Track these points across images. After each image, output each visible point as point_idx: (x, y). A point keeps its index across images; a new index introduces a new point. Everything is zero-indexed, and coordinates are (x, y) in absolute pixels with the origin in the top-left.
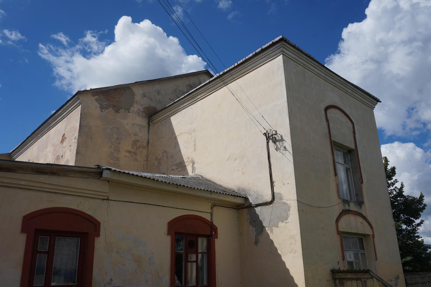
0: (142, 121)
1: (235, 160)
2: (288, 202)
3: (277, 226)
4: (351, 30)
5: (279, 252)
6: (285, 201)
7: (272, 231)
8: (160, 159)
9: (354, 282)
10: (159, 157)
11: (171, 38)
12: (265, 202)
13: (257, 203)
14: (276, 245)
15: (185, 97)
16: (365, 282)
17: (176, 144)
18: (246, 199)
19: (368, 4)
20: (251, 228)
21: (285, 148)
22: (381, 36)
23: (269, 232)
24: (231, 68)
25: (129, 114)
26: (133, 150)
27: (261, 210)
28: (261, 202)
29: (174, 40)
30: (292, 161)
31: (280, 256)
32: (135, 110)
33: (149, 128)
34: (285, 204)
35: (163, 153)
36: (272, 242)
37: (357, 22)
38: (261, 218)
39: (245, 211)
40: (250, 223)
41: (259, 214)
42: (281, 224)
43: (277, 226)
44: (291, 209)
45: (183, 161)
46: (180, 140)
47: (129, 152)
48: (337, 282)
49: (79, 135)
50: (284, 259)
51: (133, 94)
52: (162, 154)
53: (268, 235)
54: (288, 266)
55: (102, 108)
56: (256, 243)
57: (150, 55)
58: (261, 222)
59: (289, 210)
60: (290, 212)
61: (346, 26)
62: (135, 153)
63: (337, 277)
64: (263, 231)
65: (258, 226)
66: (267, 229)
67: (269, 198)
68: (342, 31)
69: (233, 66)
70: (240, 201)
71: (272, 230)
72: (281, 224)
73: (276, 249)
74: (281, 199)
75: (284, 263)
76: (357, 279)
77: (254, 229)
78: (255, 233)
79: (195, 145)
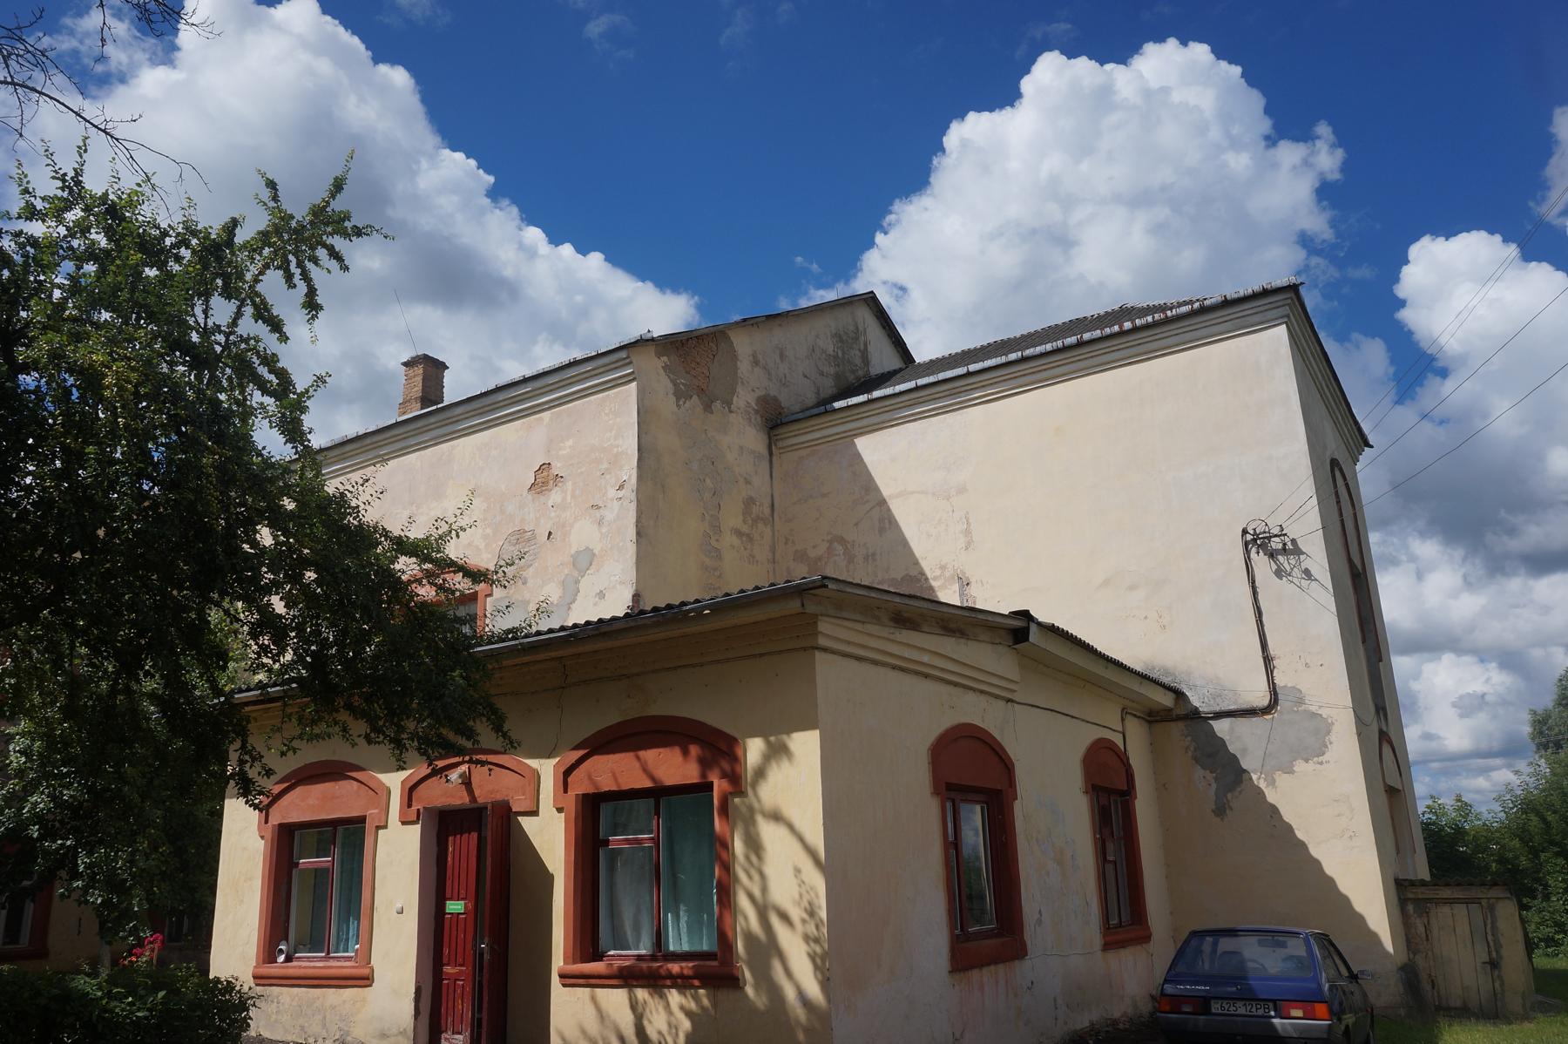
0: (753, 438)
1: (1132, 588)
2: (1324, 712)
3: (1290, 771)
4: (970, 132)
5: (1300, 835)
6: (1313, 709)
7: (1272, 783)
8: (820, 559)
9: (1461, 910)
10: (812, 554)
11: (383, 68)
12: (1244, 706)
13: (1217, 709)
14: (1288, 815)
15: (917, 388)
16: (1492, 908)
17: (887, 523)
18: (1179, 695)
19: (1033, 61)
20: (1199, 772)
21: (1307, 572)
22: (1053, 163)
23: (1262, 785)
24: (1108, 331)
25: (732, 417)
26: (745, 529)
27: (1232, 730)
28: (1232, 707)
29: (398, 77)
30: (1334, 609)
31: (1302, 846)
32: (742, 404)
33: (771, 462)
34: (1314, 715)
35: (831, 542)
36: (1274, 810)
37: (980, 109)
38: (1231, 749)
39: (1177, 729)
40: (1196, 759)
41: (1226, 738)
42: (1300, 766)
43: (1290, 771)
44: (1335, 728)
45: (922, 573)
46: (899, 510)
47: (739, 533)
48: (1410, 908)
49: (640, 478)
50: (1314, 852)
51: (734, 356)
52: (825, 546)
53: (1260, 793)
54: (1330, 869)
55: (679, 395)
56: (1220, 810)
57: (317, 120)
58: (1234, 759)
59: (1329, 732)
60: (1333, 737)
61: (962, 116)
62: (750, 538)
63: (1410, 896)
64: (1241, 782)
65: (1228, 771)
66: (1254, 777)
67: (1262, 699)
68: (944, 129)
69: (1116, 328)
70: (1167, 700)
71: (1274, 781)
72: (1300, 766)
73: (1289, 829)
74: (1300, 701)
75: (1317, 863)
76: (1467, 902)
77: (1210, 777)
78: (1214, 785)
79: (967, 532)
